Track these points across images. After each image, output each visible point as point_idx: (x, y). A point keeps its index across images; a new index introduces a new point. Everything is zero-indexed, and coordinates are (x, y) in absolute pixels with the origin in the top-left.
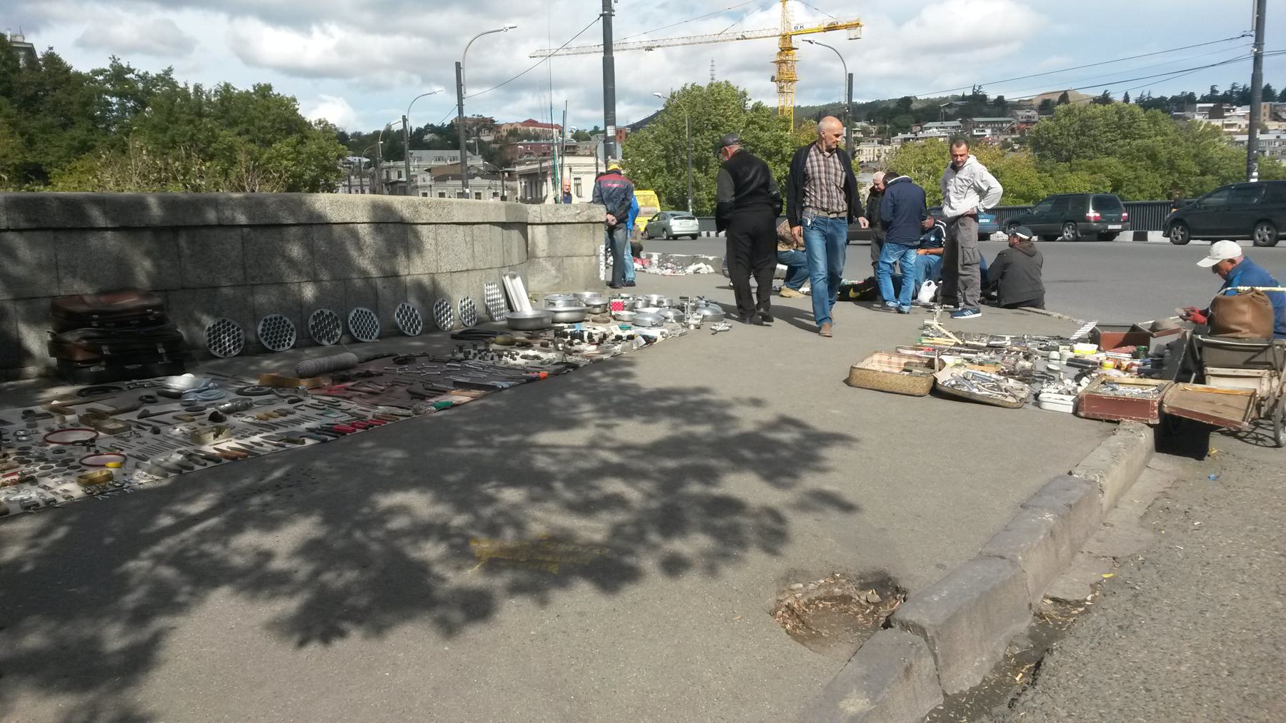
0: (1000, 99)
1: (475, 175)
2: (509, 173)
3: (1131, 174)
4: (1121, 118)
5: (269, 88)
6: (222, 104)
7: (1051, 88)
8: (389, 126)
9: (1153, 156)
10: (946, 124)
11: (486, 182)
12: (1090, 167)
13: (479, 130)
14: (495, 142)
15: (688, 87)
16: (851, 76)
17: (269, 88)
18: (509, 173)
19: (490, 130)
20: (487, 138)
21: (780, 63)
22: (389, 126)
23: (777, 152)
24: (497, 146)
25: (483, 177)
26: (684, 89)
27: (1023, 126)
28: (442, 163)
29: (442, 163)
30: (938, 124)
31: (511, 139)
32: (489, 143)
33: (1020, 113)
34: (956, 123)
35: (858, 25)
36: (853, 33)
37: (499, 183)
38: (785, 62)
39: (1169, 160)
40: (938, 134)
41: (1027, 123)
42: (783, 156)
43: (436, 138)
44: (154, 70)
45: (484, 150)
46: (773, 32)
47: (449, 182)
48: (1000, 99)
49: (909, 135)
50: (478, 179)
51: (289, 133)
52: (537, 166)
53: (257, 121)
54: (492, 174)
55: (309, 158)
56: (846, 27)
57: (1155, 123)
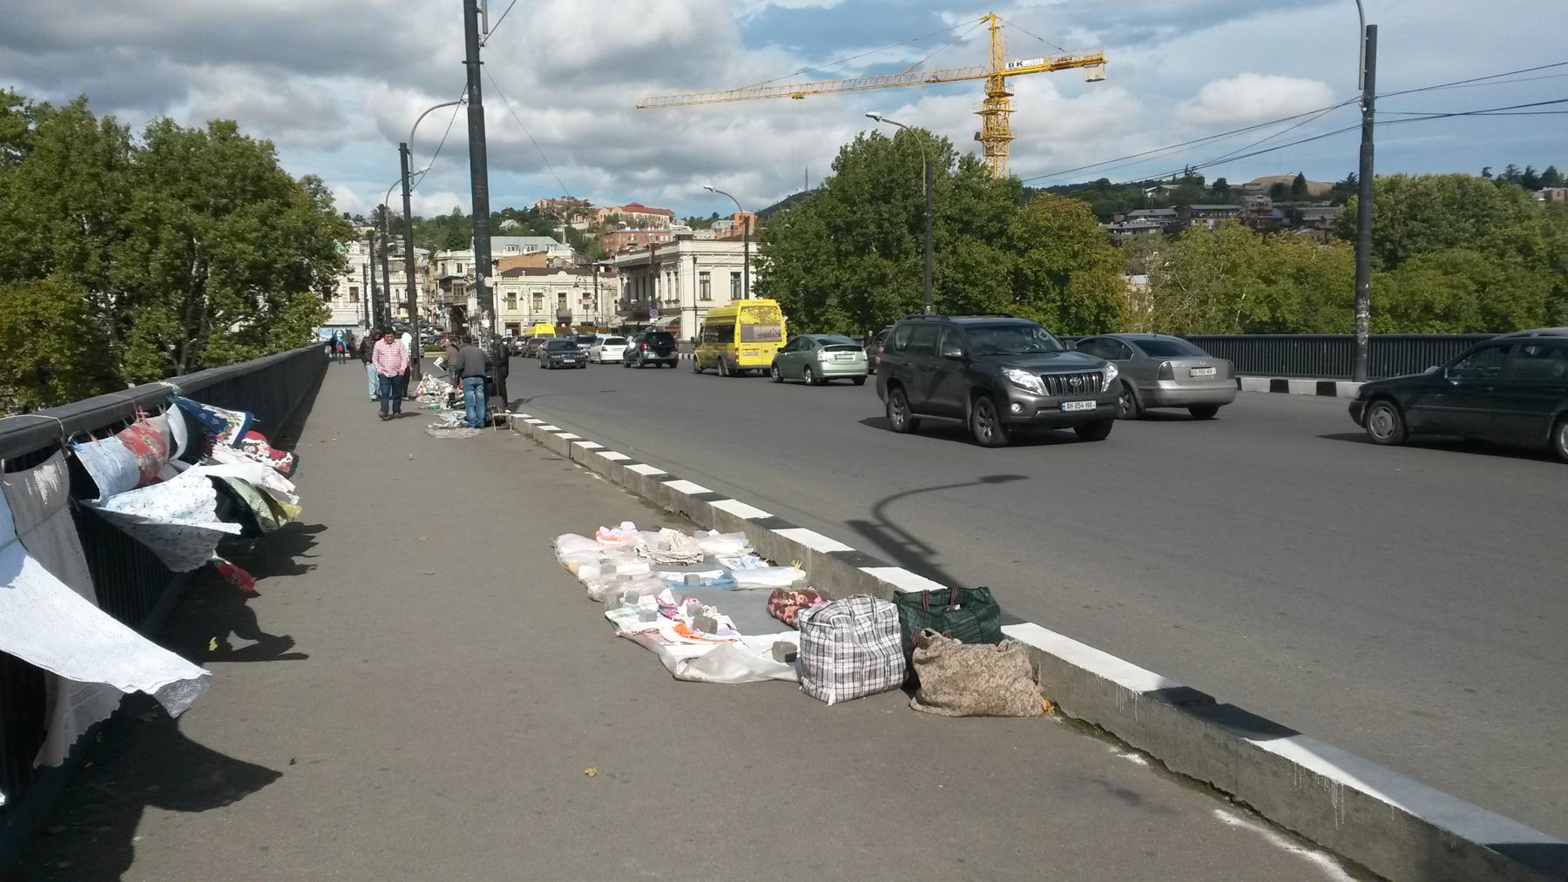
0: (1221, 184)
1: (560, 269)
2: (606, 267)
3: (1501, 276)
4: (1464, 194)
5: (232, 127)
6: (157, 152)
7: (1284, 172)
8: (457, 210)
9: (1525, 249)
10: (1158, 212)
11: (573, 278)
12: (1439, 266)
13: (570, 216)
14: (590, 231)
15: (867, 137)
16: (1371, 32)
17: (232, 127)
18: (606, 267)
19: (584, 215)
20: (580, 225)
21: (989, 114)
22: (457, 210)
23: (1001, 232)
24: (592, 236)
25: (569, 272)
26: (860, 140)
27: (1254, 216)
28: (516, 253)
29: (516, 253)
30: (1147, 212)
31: (609, 227)
32: (583, 231)
33: (1248, 198)
34: (1170, 211)
35: (1100, 61)
36: (1093, 72)
37: (590, 279)
38: (994, 113)
39: (1551, 255)
40: (1149, 224)
41: (1258, 212)
42: (1010, 239)
43: (516, 225)
44: (59, 98)
45: (574, 238)
46: (977, 72)
47: (522, 278)
48: (1221, 184)
49: (1112, 225)
50: (562, 274)
51: (258, 196)
52: (647, 255)
53: (203, 176)
54: (585, 269)
55: (286, 236)
56: (1084, 64)
57: (1514, 201)
